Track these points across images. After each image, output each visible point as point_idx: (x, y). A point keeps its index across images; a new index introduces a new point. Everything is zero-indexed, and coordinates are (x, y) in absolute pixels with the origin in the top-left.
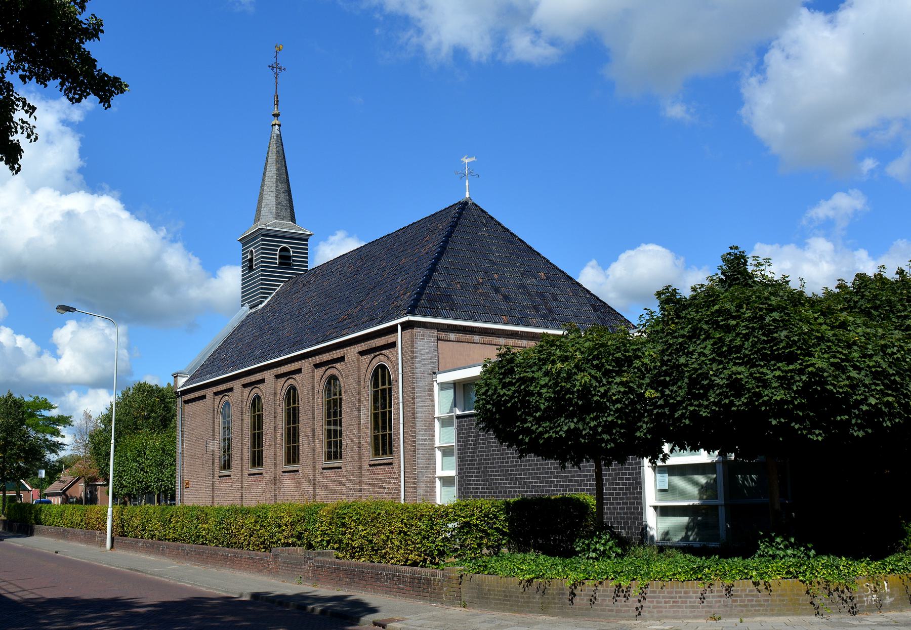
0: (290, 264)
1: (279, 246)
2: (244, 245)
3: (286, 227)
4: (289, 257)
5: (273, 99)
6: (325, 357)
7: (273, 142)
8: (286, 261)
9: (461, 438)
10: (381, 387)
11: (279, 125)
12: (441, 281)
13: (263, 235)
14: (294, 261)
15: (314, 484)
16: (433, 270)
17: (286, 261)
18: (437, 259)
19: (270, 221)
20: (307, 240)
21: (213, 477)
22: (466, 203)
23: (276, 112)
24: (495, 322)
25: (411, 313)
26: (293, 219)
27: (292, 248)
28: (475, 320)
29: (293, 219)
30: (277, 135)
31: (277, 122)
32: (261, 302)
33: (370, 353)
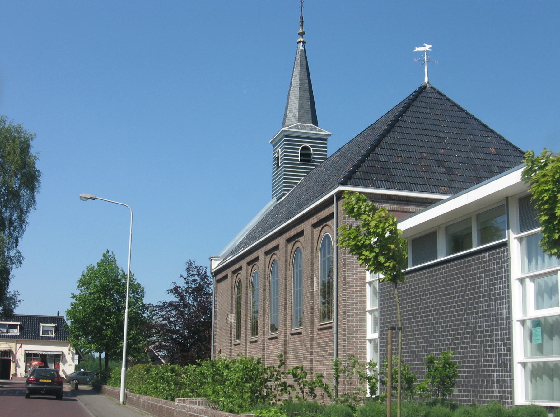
0: (310, 161)
1: (300, 145)
2: (274, 146)
3: (308, 129)
4: (310, 155)
5: (298, 20)
6: (293, 232)
7: (298, 57)
8: (306, 157)
9: (382, 301)
10: (327, 256)
11: (304, 42)
12: (381, 154)
13: (286, 136)
14: (314, 158)
15: (285, 349)
16: (378, 143)
17: (306, 157)
18: (383, 136)
19: (293, 124)
20: (326, 140)
21: (231, 346)
22: (425, 87)
23: (301, 31)
24: (432, 192)
25: (344, 183)
26: (315, 122)
27: (312, 146)
28: (410, 190)
29: (315, 122)
30: (301, 51)
31: (302, 40)
32: (284, 194)
33: (319, 226)
